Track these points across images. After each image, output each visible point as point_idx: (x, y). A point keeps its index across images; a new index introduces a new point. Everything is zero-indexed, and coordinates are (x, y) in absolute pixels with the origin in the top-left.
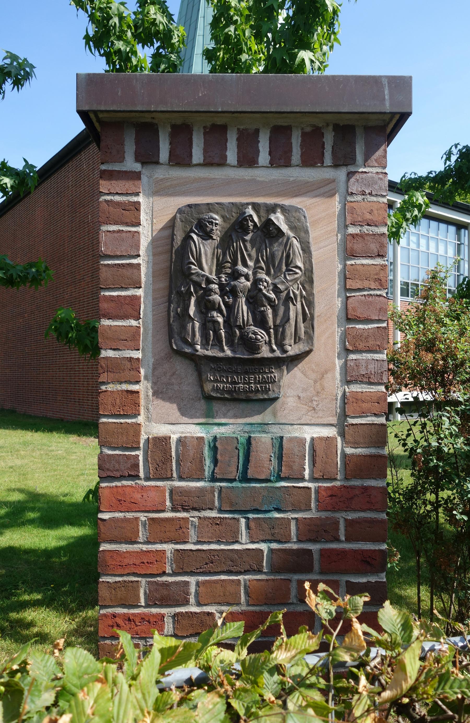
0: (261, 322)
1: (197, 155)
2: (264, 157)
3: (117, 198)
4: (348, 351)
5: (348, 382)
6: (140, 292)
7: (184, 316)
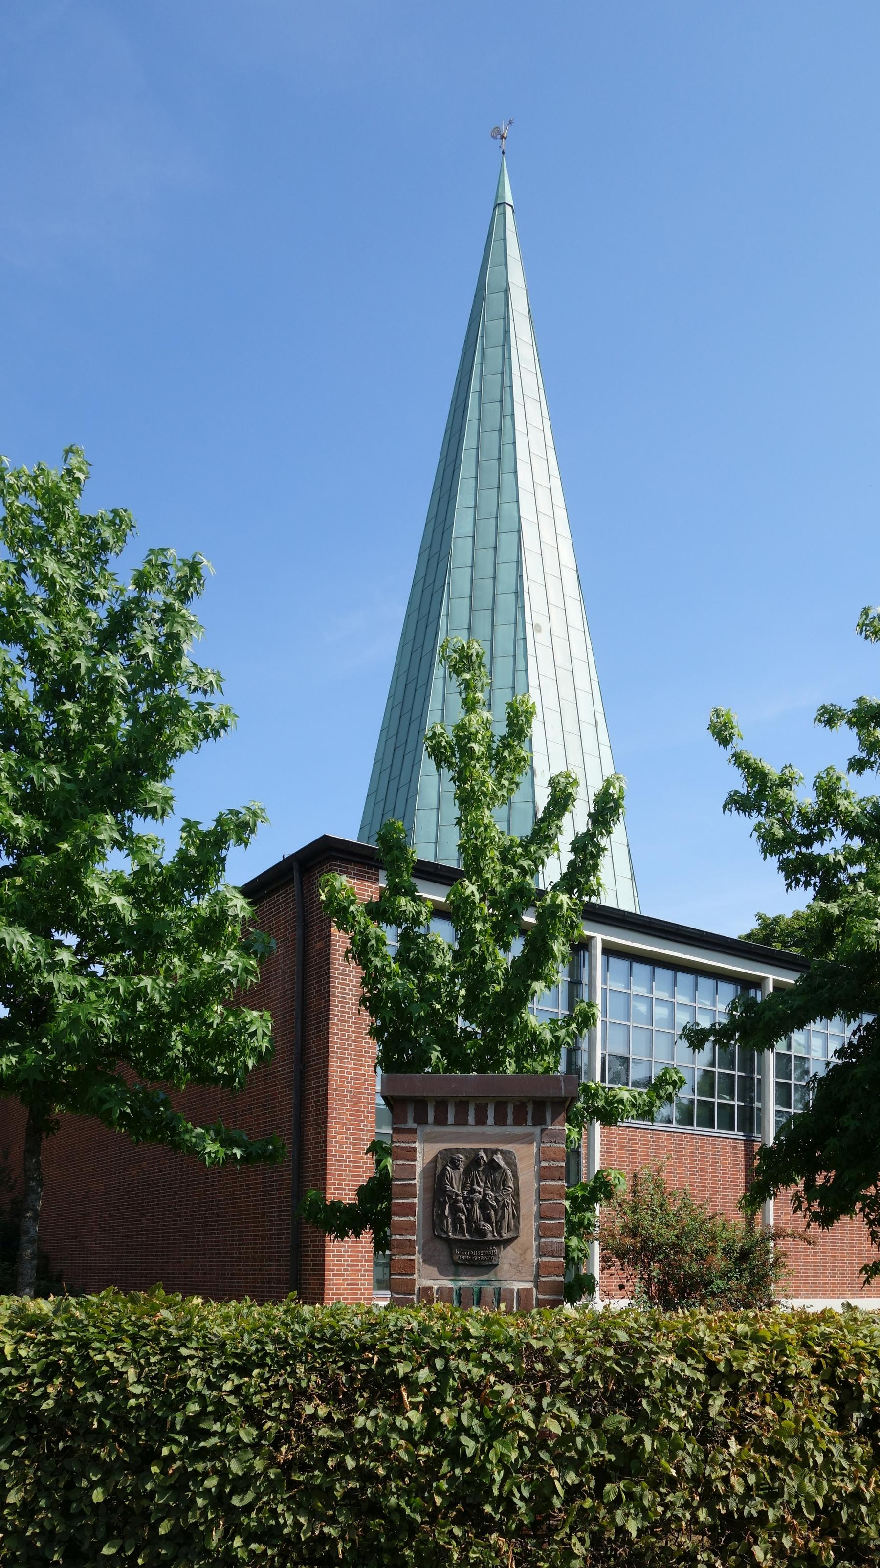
0: (488, 1219)
1: (451, 1118)
2: (491, 1120)
3: (403, 1145)
4: (541, 1237)
5: (541, 1256)
6: (416, 1201)
7: (442, 1215)
